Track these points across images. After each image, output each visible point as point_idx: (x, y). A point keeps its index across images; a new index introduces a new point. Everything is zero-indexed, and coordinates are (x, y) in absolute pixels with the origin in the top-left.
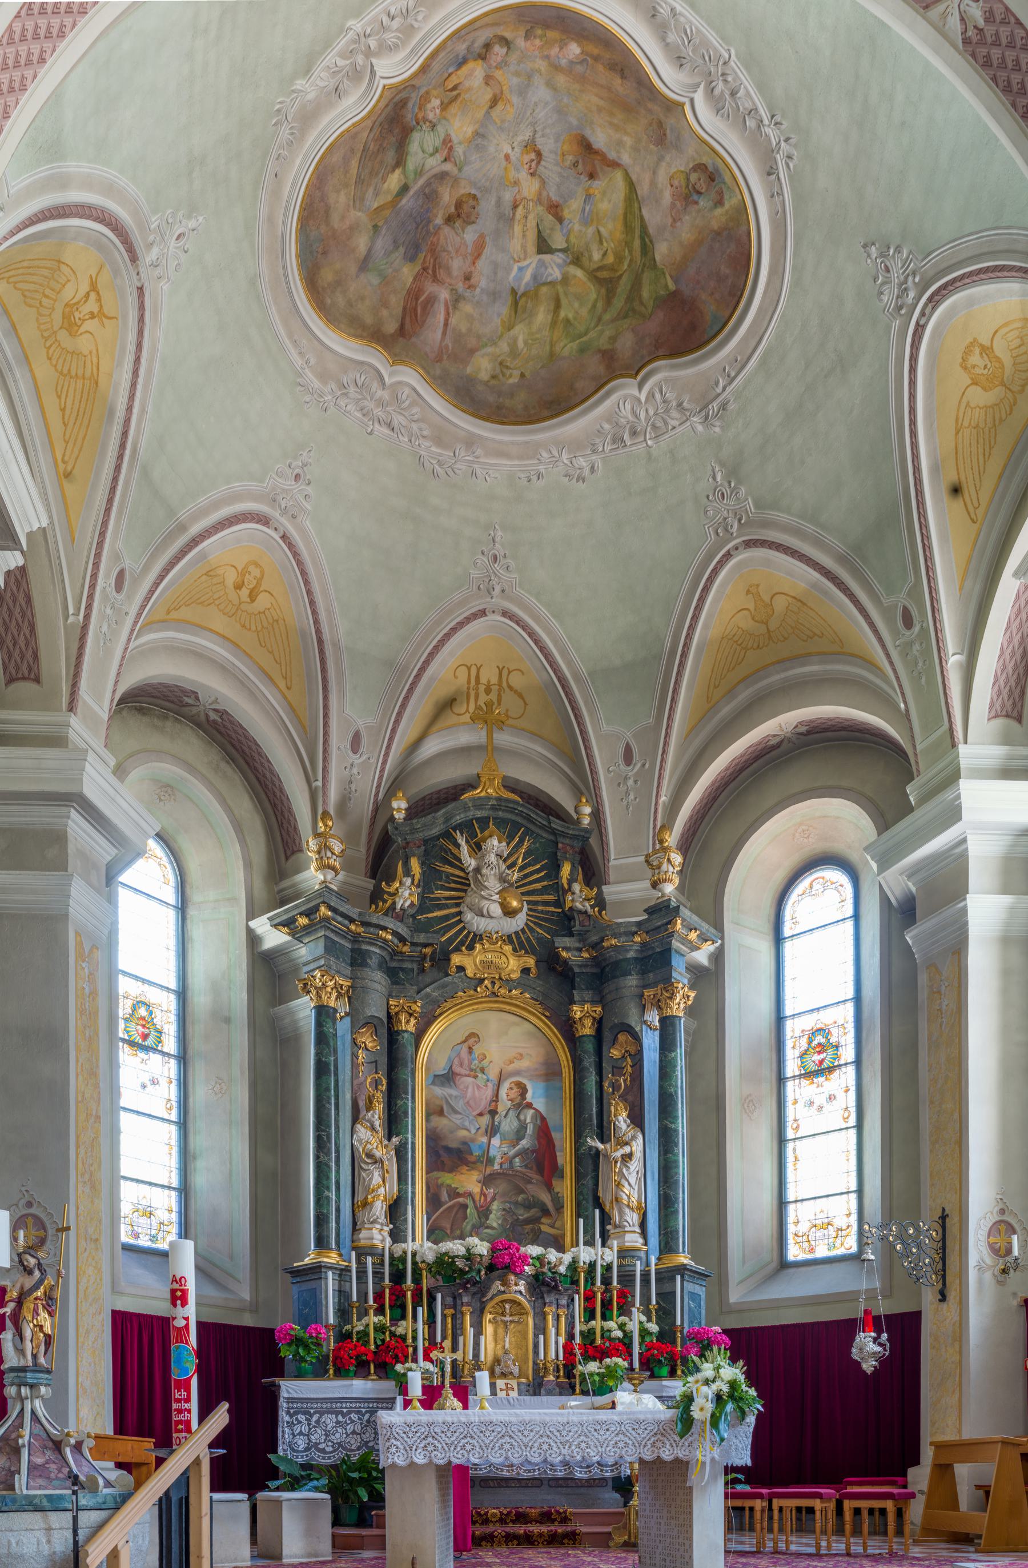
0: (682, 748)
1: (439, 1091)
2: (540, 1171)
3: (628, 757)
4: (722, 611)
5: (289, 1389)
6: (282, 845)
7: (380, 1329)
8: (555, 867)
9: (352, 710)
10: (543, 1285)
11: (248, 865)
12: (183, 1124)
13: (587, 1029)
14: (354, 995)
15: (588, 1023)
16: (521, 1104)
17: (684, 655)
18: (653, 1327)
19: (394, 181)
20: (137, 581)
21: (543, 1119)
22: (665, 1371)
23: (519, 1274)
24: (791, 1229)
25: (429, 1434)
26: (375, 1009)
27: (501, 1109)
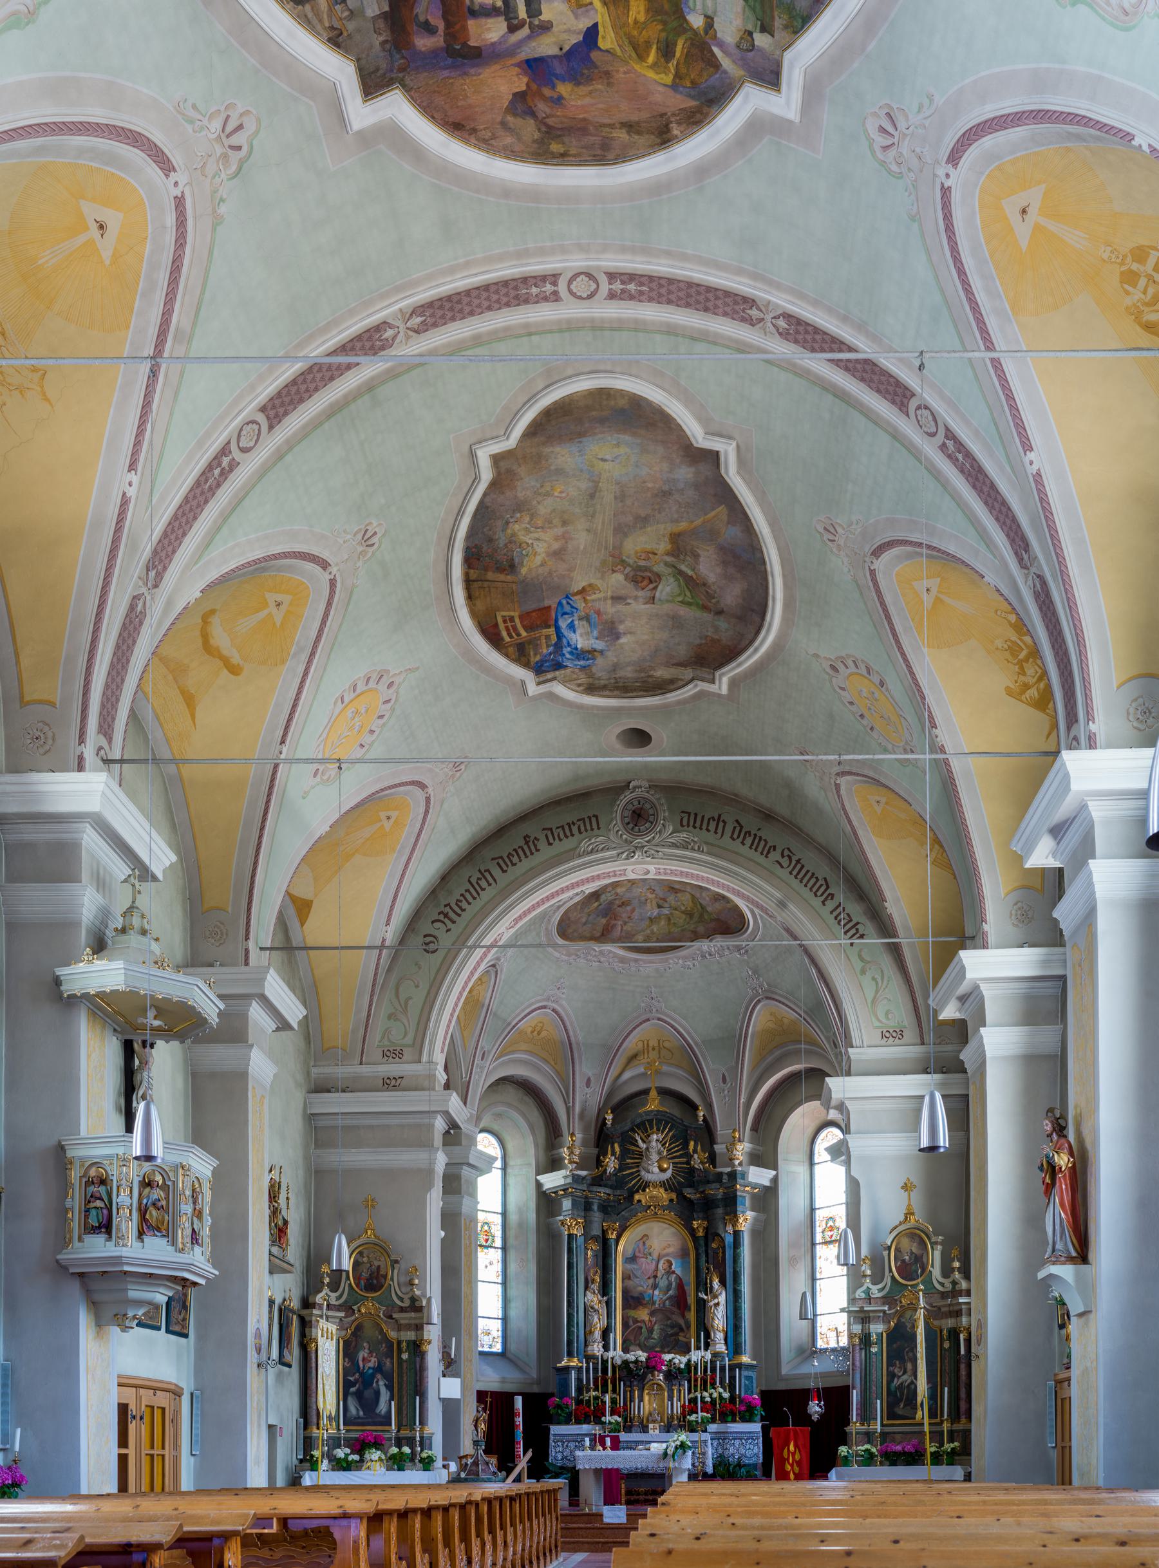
0: (753, 1069)
1: (628, 1266)
2: (679, 1308)
3: (724, 1080)
4: (760, 1019)
5: (555, 1429)
6: (553, 1132)
7: (596, 1398)
8: (685, 1145)
9: (585, 1068)
10: (673, 1375)
11: (536, 1145)
12: (504, 1284)
13: (701, 1233)
14: (586, 1227)
15: (701, 1230)
16: (669, 1272)
17: (746, 1037)
18: (726, 1395)
19: (596, 904)
20: (489, 1052)
21: (680, 1279)
22: (730, 1418)
23: (660, 1371)
24: (819, 1330)
25: (590, 1459)
26: (596, 1231)
27: (659, 1275)
